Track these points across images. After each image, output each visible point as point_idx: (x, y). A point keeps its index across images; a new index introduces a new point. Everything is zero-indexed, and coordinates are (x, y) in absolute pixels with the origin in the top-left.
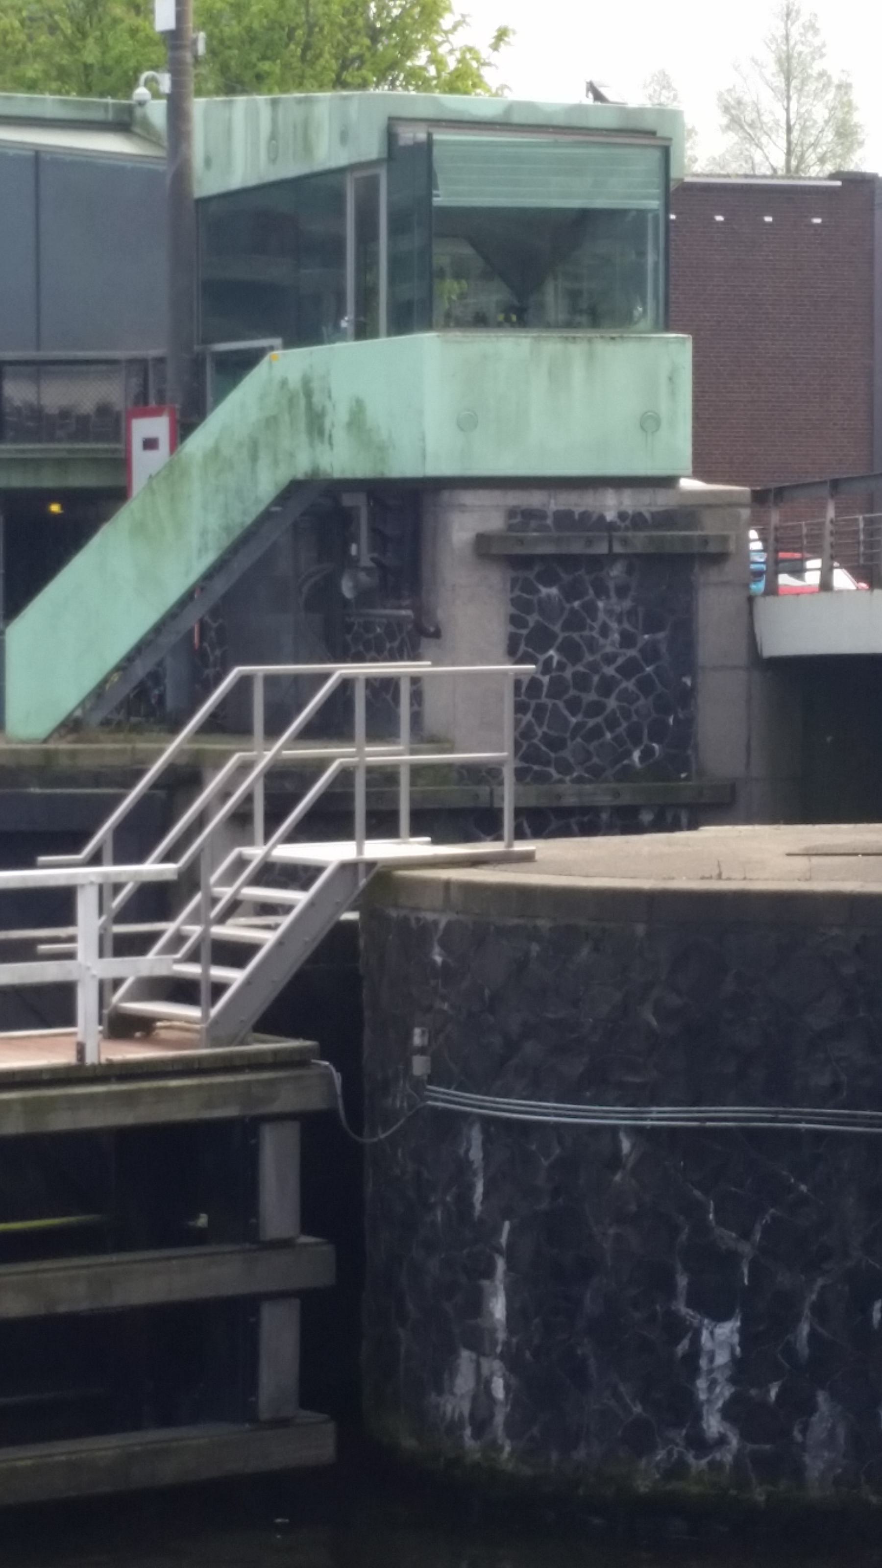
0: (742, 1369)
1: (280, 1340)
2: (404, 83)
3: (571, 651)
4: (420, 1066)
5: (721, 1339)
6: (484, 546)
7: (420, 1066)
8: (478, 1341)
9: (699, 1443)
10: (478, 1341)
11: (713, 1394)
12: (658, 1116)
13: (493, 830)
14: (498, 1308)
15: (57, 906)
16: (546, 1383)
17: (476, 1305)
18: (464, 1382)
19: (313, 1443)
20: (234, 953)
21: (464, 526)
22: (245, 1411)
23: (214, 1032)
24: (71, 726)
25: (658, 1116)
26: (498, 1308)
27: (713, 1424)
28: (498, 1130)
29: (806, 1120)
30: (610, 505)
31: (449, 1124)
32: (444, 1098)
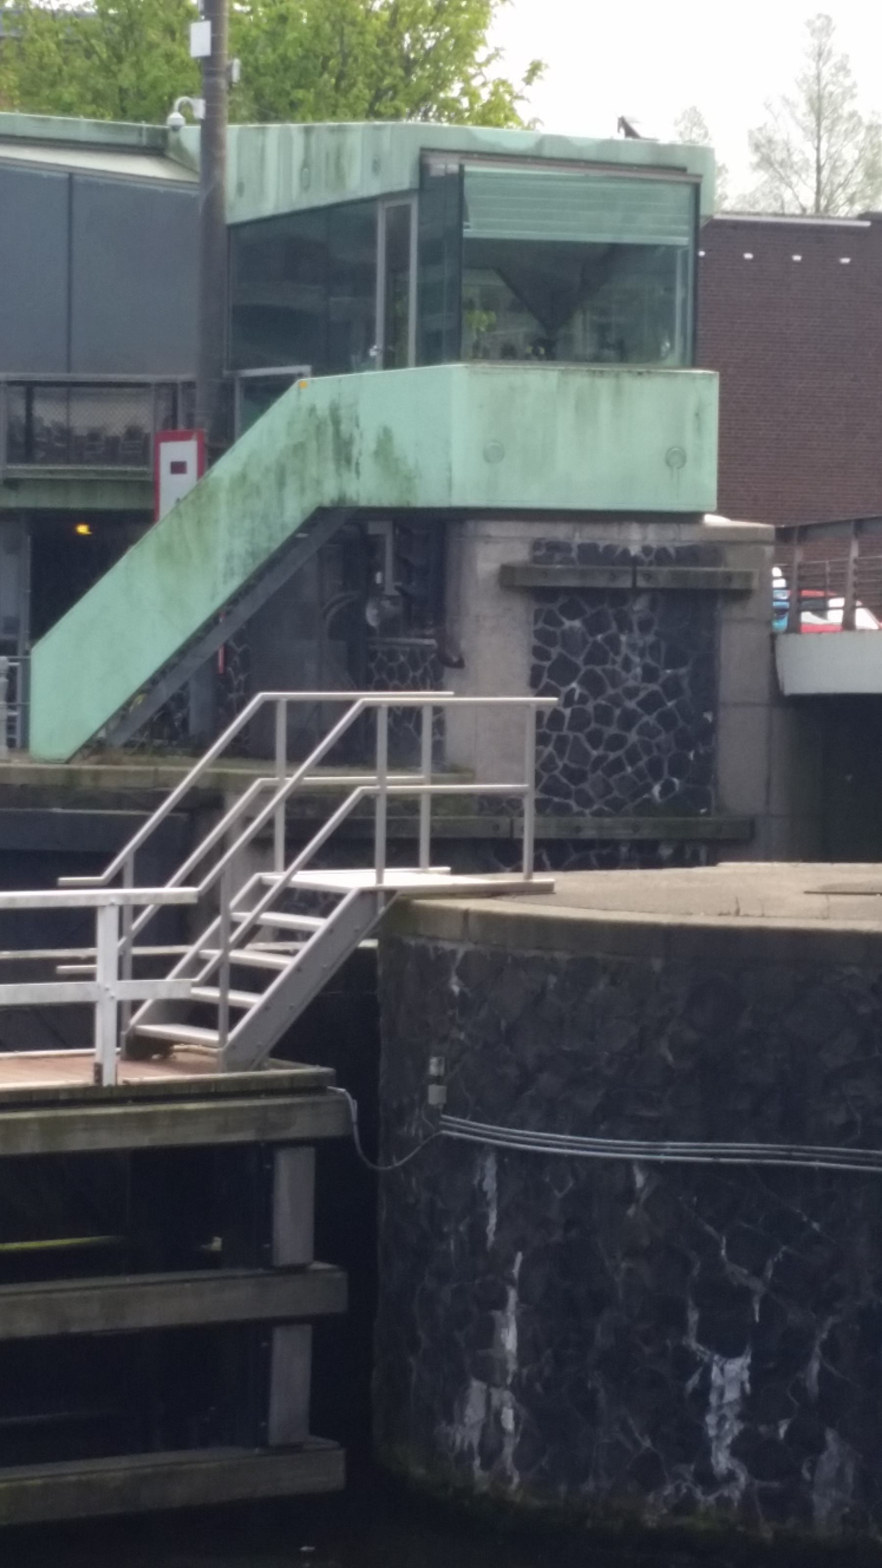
0: (752, 1407)
1: (291, 1364)
3: (593, 684)
4: (435, 1095)
5: (731, 1375)
6: (509, 579)
7: (435, 1095)
8: (488, 1372)
9: (707, 1478)
10: (488, 1372)
11: (722, 1430)
12: (673, 1151)
13: (512, 862)
15: (78, 926)
17: (488, 1333)
18: (474, 1412)
19: (323, 1470)
20: (253, 978)
21: (489, 557)
23: (232, 1056)
24: (95, 747)
25: (673, 1151)
26: (510, 1339)
27: (722, 1461)
29: (821, 1158)
31: (465, 1153)
32: (459, 1127)
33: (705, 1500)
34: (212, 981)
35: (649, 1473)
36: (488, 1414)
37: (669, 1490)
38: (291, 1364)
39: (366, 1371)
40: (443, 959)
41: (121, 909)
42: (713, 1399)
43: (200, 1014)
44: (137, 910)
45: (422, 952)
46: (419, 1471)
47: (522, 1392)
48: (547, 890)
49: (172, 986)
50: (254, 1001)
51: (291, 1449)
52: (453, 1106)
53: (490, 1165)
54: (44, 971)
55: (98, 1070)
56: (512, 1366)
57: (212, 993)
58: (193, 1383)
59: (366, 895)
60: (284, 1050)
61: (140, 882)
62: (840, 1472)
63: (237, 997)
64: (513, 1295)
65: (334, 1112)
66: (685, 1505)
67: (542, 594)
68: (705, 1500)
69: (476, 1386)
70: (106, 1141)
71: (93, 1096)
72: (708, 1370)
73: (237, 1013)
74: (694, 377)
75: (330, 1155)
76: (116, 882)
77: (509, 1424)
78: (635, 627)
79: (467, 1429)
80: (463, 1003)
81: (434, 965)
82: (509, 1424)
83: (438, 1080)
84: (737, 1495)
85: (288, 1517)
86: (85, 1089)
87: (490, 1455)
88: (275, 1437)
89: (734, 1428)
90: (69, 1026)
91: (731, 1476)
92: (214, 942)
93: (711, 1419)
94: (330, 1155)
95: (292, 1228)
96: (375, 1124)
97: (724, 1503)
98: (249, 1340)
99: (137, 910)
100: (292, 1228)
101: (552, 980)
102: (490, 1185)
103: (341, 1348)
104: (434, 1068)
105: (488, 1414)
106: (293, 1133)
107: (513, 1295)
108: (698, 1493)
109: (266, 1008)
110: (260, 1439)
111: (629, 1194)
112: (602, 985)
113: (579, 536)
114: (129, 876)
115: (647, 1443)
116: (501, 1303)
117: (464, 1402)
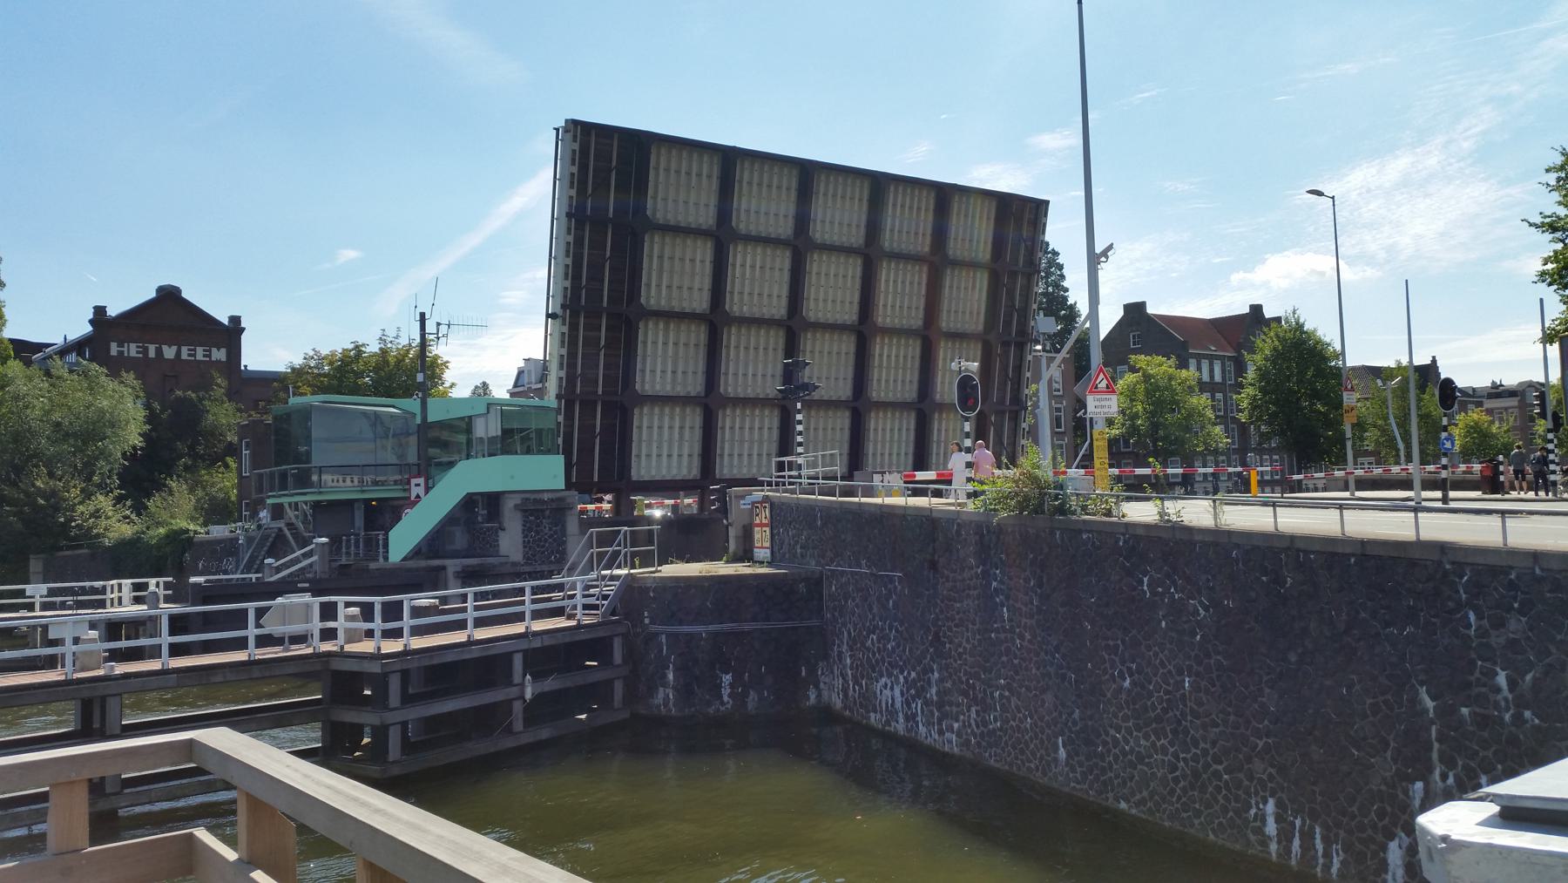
0: (732, 685)
1: (619, 687)
2: (1444, 461)
3: (537, 533)
4: (647, 621)
5: (727, 678)
6: (516, 506)
7: (647, 621)
8: (665, 685)
9: (723, 703)
10: (665, 685)
11: (726, 692)
12: (711, 628)
13: (1410, 488)
14: (671, 676)
15: (521, 591)
16: (685, 692)
17: (664, 676)
18: (661, 695)
19: (625, 715)
20: (605, 597)
21: (509, 504)
22: (509, 731)
23: (604, 615)
24: (405, 559)
25: (711, 628)
26: (671, 676)
27: (726, 698)
28: (669, 635)
29: (746, 627)
30: (546, 497)
31: (657, 634)
32: (653, 628)
38: (619, 687)
67: (525, 511)
70: (583, 637)
78: (1101, 455)
95: (618, 657)
100: (618, 657)
113: (533, 496)
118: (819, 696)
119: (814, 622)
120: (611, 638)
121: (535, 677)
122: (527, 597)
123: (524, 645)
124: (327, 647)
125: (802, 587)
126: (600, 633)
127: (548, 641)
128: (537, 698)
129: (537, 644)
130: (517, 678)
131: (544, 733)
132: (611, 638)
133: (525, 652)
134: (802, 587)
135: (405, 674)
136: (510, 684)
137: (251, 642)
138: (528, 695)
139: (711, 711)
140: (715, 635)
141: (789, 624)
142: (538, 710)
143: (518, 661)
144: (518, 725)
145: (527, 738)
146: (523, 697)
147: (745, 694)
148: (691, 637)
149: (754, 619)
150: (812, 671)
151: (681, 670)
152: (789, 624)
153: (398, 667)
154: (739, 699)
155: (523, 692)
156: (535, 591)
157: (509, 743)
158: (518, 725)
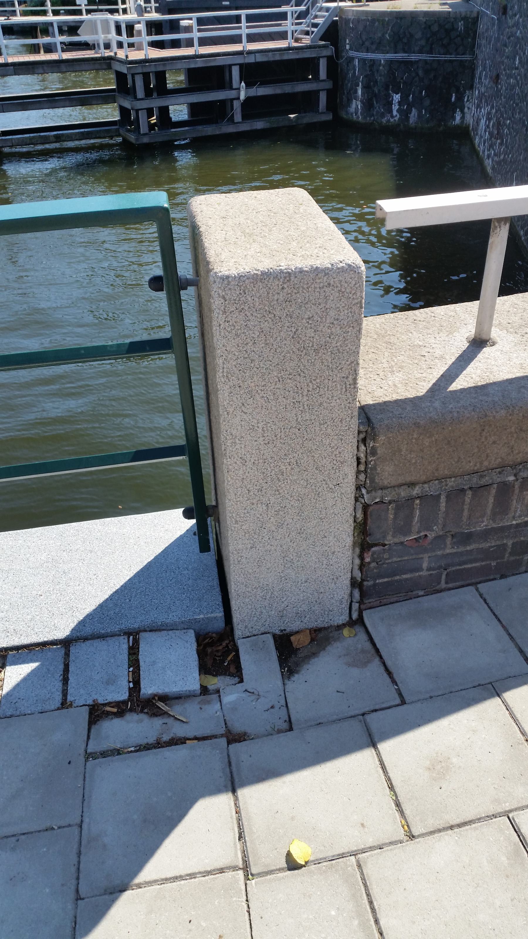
0: (400, 103)
1: (323, 98)
4: (348, 47)
5: (397, 98)
7: (348, 47)
9: (392, 117)
11: (395, 108)
12: (390, 56)
14: (360, 92)
16: (368, 105)
17: (356, 92)
18: (354, 106)
19: (329, 117)
20: (315, 25)
22: (231, 120)
26: (360, 92)
27: (395, 113)
28: (363, 61)
29: (414, 57)
31: (352, 59)
32: (352, 54)
33: (392, 120)
34: (308, 26)
35: (383, 115)
36: (356, 107)
37: (386, 119)
39: (337, 97)
40: (349, 20)
41: (292, 12)
42: (394, 102)
43: (307, 33)
44: (296, 12)
45: (346, 19)
46: (345, 116)
47: (362, 102)
48: (368, 5)
49: (303, 27)
50: (315, 30)
51: (323, 113)
52: (351, 49)
53: (357, 60)
54: (280, 25)
55: (289, 43)
56: (360, 97)
57: (308, 29)
58: (307, 101)
59: (335, 8)
60: (321, 39)
61: (296, 6)
62: (415, 114)
63: (313, 29)
64: (360, 84)
65: (330, 51)
66: (388, 121)
68: (392, 120)
69: (354, 100)
71: (289, 49)
72: (393, 97)
73: (313, 32)
74: (370, 884)
75: (330, 59)
76: (292, 6)
77: (359, 108)
79: (352, 109)
80: (353, 29)
81: (347, 21)
82: (359, 108)
83: (348, 44)
84: (397, 119)
85: (323, 125)
86: (287, 47)
87: (356, 113)
88: (320, 111)
89: (397, 107)
90: (283, 36)
91: (396, 116)
92: (308, 19)
93: (393, 106)
94: (330, 59)
95: (323, 74)
96: (338, 52)
97: (395, 120)
98: (316, 93)
99: (296, 12)
100: (323, 74)
101: (368, 23)
102: (357, 64)
103: (332, 95)
104: (347, 42)
105: (356, 107)
106: (323, 55)
107: (360, 84)
108: (391, 119)
109: (318, 31)
110: (319, 112)
111: (380, 65)
112: (377, 23)
114: (294, 5)
115: (382, 110)
116: (358, 86)
117: (352, 104)
118: (463, 118)
119: (467, 57)
120: (318, 59)
121: (248, 85)
122: (244, 23)
123: (240, 60)
124: (108, 53)
125: (461, 25)
126: (307, 55)
127: (260, 58)
128: (248, 99)
129: (251, 59)
130: (235, 85)
131: (259, 125)
132: (318, 59)
133: (241, 66)
134: (461, 25)
135: (146, 76)
136: (231, 88)
137: (244, 39)
138: (242, 97)
139: (384, 121)
140: (390, 63)
141: (448, 57)
142: (252, 108)
143: (236, 72)
144: (238, 117)
145: (246, 127)
146: (238, 98)
147: (409, 111)
148: (373, 63)
149: (421, 52)
150: (460, 98)
151: (366, 87)
152: (448, 57)
153: (140, 70)
154: (405, 114)
155: (239, 94)
156: (201, 21)
157: (230, 129)
158: (238, 117)
